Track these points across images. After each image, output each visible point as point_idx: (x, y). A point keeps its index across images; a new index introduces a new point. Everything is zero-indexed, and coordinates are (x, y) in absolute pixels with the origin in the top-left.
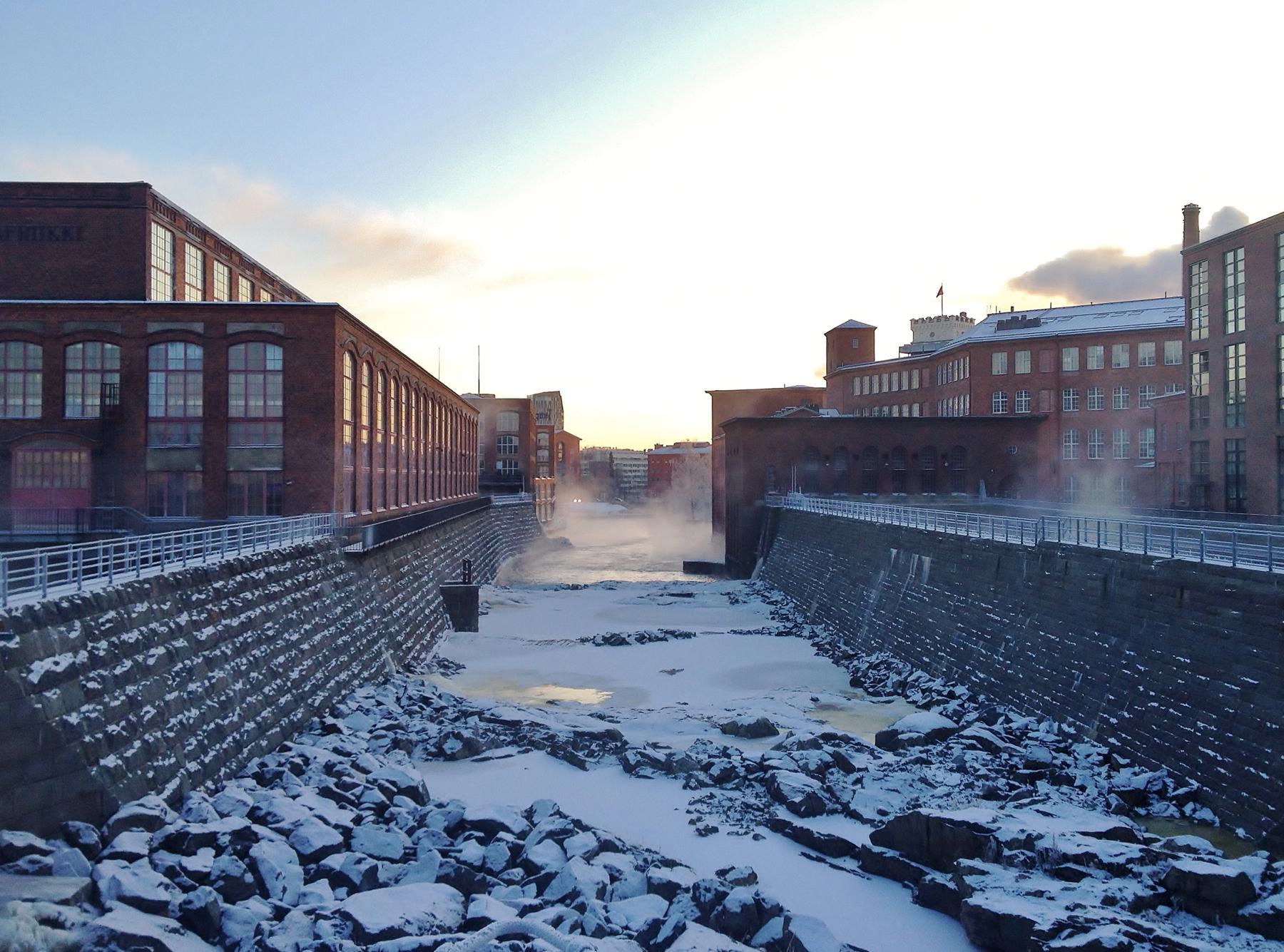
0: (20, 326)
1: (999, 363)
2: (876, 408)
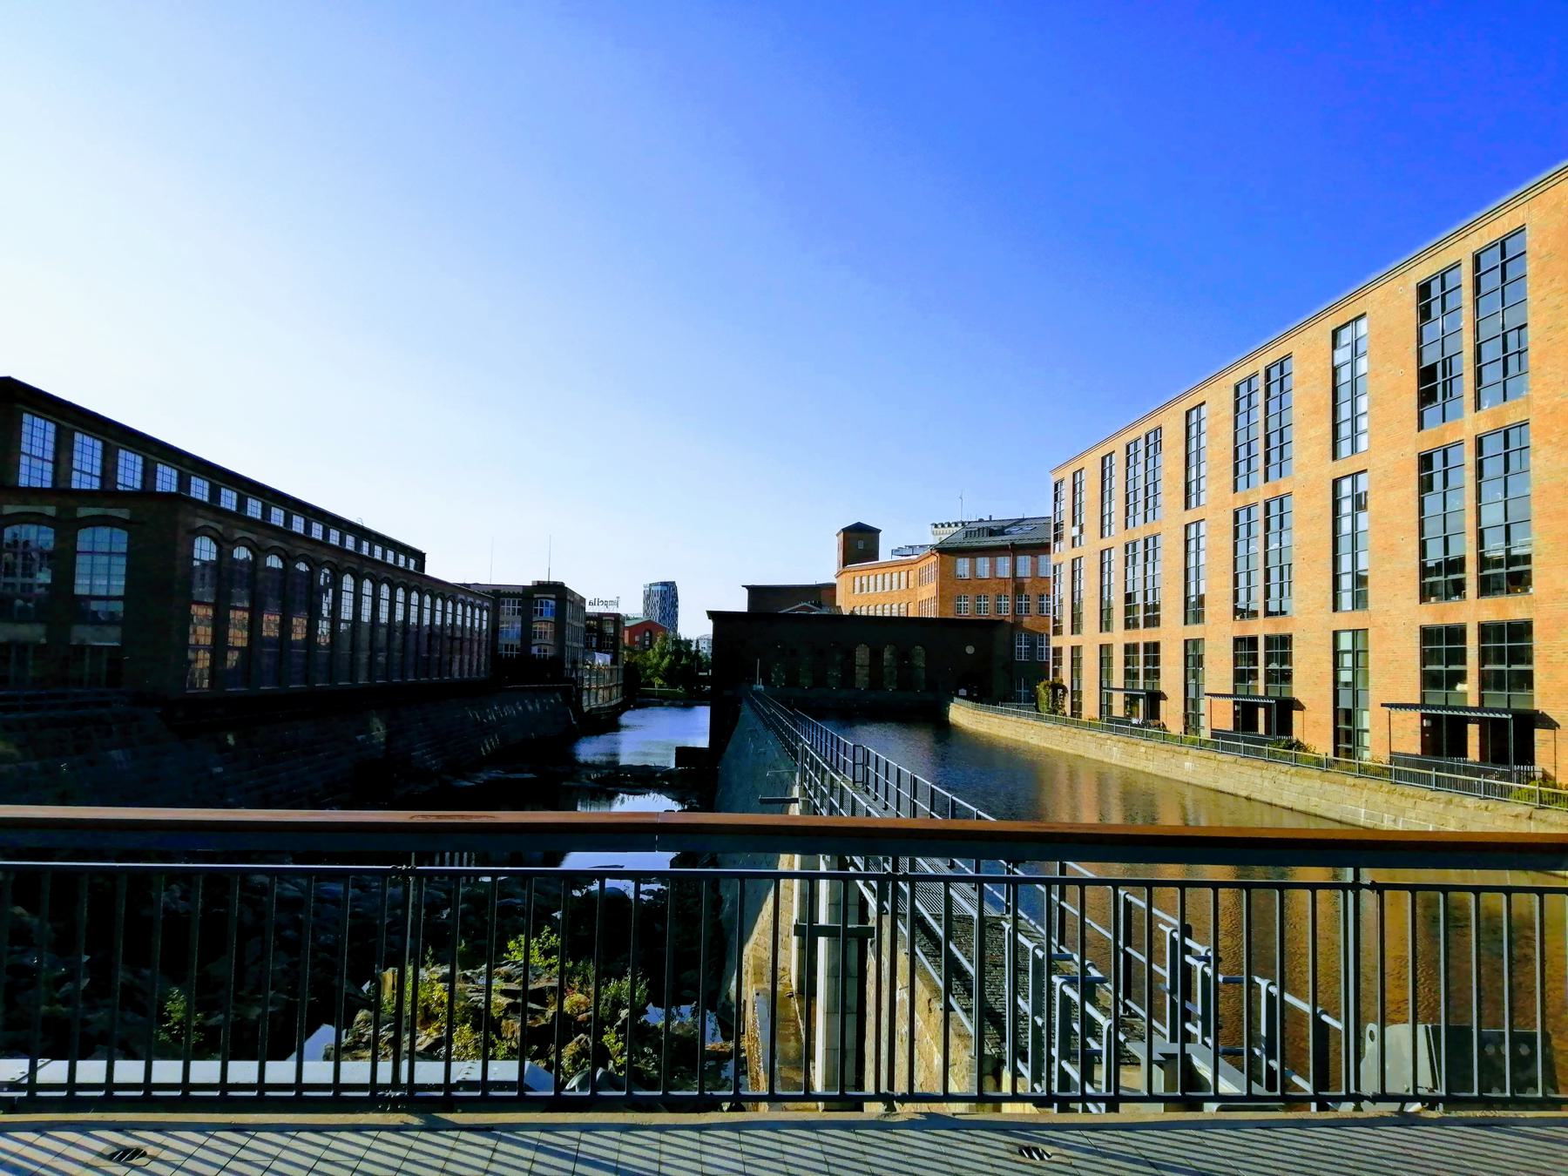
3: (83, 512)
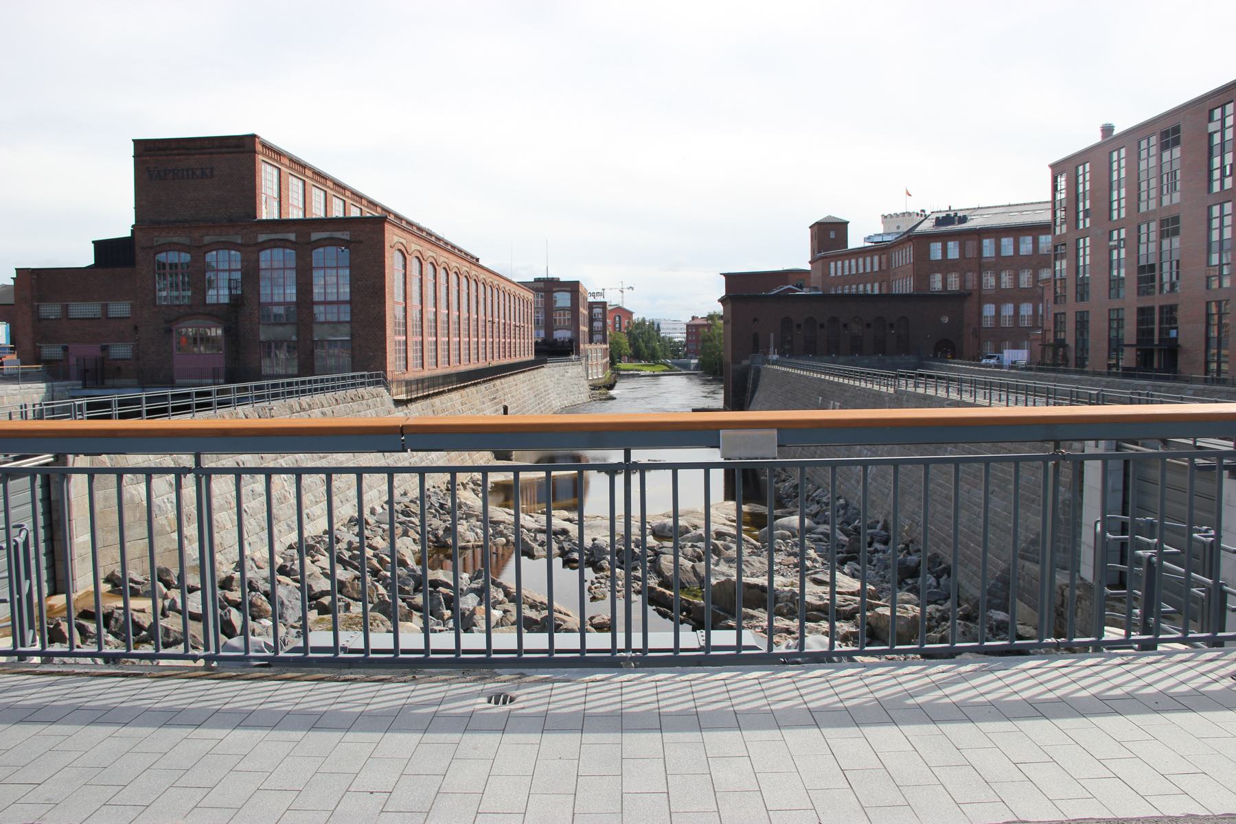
0: (176, 239)
1: (936, 251)
2: (847, 287)
3: (315, 236)
